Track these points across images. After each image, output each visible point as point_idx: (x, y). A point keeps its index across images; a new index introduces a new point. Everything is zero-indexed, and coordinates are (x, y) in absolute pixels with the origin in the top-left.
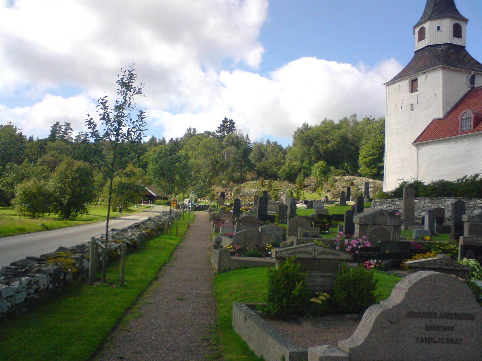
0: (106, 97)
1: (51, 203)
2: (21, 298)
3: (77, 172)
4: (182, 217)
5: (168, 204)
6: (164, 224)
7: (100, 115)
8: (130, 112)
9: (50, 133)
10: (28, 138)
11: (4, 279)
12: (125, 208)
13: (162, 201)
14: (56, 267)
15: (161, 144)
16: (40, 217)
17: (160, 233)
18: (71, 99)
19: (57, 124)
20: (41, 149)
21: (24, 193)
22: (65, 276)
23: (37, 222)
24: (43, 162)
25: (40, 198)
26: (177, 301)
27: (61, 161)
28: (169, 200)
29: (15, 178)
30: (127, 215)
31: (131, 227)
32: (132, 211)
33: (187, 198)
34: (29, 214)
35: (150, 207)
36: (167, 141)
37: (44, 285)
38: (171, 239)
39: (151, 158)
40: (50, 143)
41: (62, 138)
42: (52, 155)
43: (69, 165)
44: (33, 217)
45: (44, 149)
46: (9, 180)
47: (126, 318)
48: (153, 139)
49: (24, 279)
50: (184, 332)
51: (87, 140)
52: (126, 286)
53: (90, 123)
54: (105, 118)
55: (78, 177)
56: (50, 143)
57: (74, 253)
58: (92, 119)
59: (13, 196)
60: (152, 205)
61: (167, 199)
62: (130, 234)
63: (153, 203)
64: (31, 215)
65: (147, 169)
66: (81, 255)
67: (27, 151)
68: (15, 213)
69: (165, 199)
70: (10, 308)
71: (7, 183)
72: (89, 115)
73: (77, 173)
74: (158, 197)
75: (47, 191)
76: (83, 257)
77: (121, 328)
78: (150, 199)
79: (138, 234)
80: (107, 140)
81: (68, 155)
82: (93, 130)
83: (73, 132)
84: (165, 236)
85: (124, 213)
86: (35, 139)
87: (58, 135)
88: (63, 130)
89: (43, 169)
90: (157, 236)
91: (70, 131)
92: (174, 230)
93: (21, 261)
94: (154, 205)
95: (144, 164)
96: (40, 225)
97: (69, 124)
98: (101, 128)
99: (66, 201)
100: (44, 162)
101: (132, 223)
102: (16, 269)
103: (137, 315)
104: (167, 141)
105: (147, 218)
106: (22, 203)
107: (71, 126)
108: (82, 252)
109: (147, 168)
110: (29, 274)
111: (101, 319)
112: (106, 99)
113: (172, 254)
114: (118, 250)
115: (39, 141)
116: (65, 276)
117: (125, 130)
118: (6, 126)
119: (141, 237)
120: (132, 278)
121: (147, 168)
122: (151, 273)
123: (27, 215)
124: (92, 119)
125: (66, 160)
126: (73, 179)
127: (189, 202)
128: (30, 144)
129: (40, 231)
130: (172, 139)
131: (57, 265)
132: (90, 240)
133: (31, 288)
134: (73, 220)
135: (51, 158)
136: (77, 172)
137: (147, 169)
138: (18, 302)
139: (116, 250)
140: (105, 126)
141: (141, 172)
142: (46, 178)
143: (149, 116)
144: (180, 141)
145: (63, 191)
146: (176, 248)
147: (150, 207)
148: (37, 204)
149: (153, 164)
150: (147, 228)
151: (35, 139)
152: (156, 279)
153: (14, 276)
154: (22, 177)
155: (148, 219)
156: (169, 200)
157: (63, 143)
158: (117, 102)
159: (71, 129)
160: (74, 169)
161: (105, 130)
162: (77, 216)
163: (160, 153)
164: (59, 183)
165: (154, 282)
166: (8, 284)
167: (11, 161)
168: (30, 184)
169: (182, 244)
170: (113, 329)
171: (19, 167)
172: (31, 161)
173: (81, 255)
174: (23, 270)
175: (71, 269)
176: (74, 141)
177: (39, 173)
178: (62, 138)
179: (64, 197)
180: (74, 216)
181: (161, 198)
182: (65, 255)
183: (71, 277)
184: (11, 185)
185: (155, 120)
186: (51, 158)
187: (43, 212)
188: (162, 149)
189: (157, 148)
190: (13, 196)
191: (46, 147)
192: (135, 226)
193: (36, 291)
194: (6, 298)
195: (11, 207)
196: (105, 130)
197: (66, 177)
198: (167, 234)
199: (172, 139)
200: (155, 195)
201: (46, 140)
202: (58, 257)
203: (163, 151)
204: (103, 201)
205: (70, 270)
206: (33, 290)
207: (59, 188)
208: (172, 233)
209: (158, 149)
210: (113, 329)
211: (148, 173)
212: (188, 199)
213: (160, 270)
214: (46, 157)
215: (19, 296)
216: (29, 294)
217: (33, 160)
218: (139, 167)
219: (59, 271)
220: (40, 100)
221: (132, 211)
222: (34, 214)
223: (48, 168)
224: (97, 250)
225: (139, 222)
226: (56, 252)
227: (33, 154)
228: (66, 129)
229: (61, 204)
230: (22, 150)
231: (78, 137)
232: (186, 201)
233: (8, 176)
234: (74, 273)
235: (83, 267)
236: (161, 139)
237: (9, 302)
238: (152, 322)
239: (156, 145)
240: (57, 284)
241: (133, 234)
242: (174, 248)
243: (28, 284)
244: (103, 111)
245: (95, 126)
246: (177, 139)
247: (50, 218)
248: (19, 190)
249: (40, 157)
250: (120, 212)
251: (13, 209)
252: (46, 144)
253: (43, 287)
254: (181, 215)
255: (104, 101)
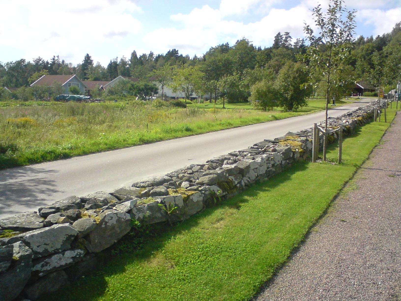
0: (320, 5)
1: (277, 99)
2: (263, 170)
3: (297, 72)
4: (389, 106)
5: (376, 95)
6: (374, 113)
7: (316, 21)
8: (341, 14)
9: (274, 42)
10: (257, 48)
11: (251, 156)
12: (337, 100)
13: (370, 93)
14: (287, 148)
15: (369, 42)
16: (269, 110)
17: (370, 120)
18: (293, 9)
19: (279, 34)
20: (268, 56)
21: (257, 92)
22: (294, 154)
23: (269, 114)
24: (270, 66)
25: (270, 95)
26: (389, 178)
27: (284, 64)
28: (376, 92)
29: (250, 81)
30: (339, 106)
31: (344, 116)
32: (344, 102)
33: (394, 89)
34: (261, 108)
35: (359, 98)
36: (374, 38)
37: (279, 161)
38: (380, 125)
39: (360, 55)
40: (274, 51)
41: (284, 45)
42: (277, 60)
43: (290, 67)
44: (264, 110)
45: (270, 56)
46: (246, 82)
47: (345, 189)
48: (362, 38)
49: (264, 156)
50: (398, 204)
51: (303, 45)
52: (343, 164)
53: (308, 30)
54: (321, 23)
55: (298, 76)
56: (274, 51)
57: (300, 136)
58: (308, 26)
59: (250, 95)
60: (360, 97)
61: (374, 91)
62: (344, 121)
63: (362, 95)
64: (263, 109)
65: (356, 66)
66: (305, 138)
67: (258, 58)
68: (252, 107)
69: (372, 91)
70: (256, 177)
71: (244, 85)
72: (306, 24)
73: (297, 73)
74: (365, 90)
75: (274, 89)
76: (307, 140)
77: (342, 197)
78: (359, 91)
79: (350, 121)
80: (321, 43)
81: (289, 59)
82: (311, 35)
83: (291, 40)
84: (374, 123)
85: (337, 105)
86: (263, 48)
87: (280, 43)
88: (284, 39)
89: (270, 72)
90: (368, 123)
91: (289, 39)
92: (382, 117)
93: (261, 143)
94: (362, 97)
95: (352, 62)
96: (270, 116)
97: (289, 33)
98: (317, 32)
99: (289, 97)
100: (270, 67)
101: (346, 112)
102: (258, 148)
103: (354, 187)
104: (374, 38)
105: (358, 108)
106: (256, 99)
107: (290, 35)
108: (306, 136)
109: (355, 64)
110: (267, 153)
111: (325, 190)
112: (320, 7)
113: (382, 138)
114: (335, 134)
115: (266, 49)
116: (294, 154)
117: (338, 30)
118: (241, 41)
119: (354, 122)
120: (348, 157)
121: (355, 64)
122: (365, 154)
123: (260, 109)
124: (308, 26)
125: (287, 63)
126: (294, 78)
127: (396, 92)
128: (260, 53)
129: (271, 121)
130: (379, 36)
131: (287, 146)
132: (313, 126)
133: (270, 163)
134: (296, 112)
135: (276, 62)
136: (297, 72)
137: (356, 66)
138: (261, 173)
139: (333, 134)
140: (320, 30)
141: (350, 68)
142: (273, 79)
143: (358, 16)
144: (387, 38)
145: (286, 90)
146: (385, 133)
147: (359, 98)
148: (268, 100)
149: (361, 60)
150: (358, 116)
151: (263, 48)
152: (368, 159)
153: (257, 154)
154: (256, 79)
155: (359, 109)
156: (376, 92)
157: (285, 50)
158: (330, 6)
159: (290, 37)
160: (295, 69)
161: (320, 33)
162: (298, 108)
163: (367, 50)
164: (283, 82)
165: (367, 162)
166: (254, 159)
167: (247, 68)
168: (261, 85)
169: (391, 129)
170: (335, 197)
171: (253, 72)
172: (260, 66)
173: (305, 138)
174: (263, 149)
175: (298, 149)
176: (293, 47)
177: (267, 75)
178: (284, 45)
179: (288, 94)
180: (296, 109)
181: (369, 90)
182: (293, 138)
183: (299, 155)
184: (248, 86)
185: (365, 19)
186: (276, 62)
187: (272, 106)
188: (369, 46)
189: (364, 46)
190: (250, 95)
191: (272, 54)
192: (348, 115)
193: (273, 165)
194: (253, 170)
195: (248, 103)
196: (320, 33)
197: (289, 76)
198: (376, 121)
199: (379, 36)
200: (363, 88)
201: (271, 48)
202: (288, 140)
203: (370, 48)
204: (318, 95)
205: (297, 150)
206: (271, 165)
207: (282, 86)
208: (381, 120)
209: (365, 47)
210: (335, 197)
211: (356, 70)
212: (395, 90)
213: (372, 151)
214: (272, 62)
215: (261, 168)
216: (268, 168)
217: (262, 66)
218: (349, 65)
219: (289, 150)
220: (267, 14)
221: (344, 102)
222: (265, 108)
223: (274, 71)
224: (318, 134)
225: (351, 111)
226: (286, 135)
227: (262, 61)
228: (286, 38)
229: (286, 99)
230: (254, 58)
231: (296, 43)
232: (393, 92)
233: (245, 79)
234: (301, 152)
235: (307, 148)
236: (369, 37)
237: (255, 172)
238: (368, 194)
239: (364, 43)
240: (288, 161)
241: (347, 121)
242: (383, 133)
243: (267, 160)
244: (318, 18)
245: (312, 32)
246: (384, 35)
247: (278, 111)
248: (253, 90)
249: (268, 63)
250: (334, 103)
251: (250, 104)
252: (271, 52)
253: (278, 163)
254: (388, 105)
255: (318, 9)
